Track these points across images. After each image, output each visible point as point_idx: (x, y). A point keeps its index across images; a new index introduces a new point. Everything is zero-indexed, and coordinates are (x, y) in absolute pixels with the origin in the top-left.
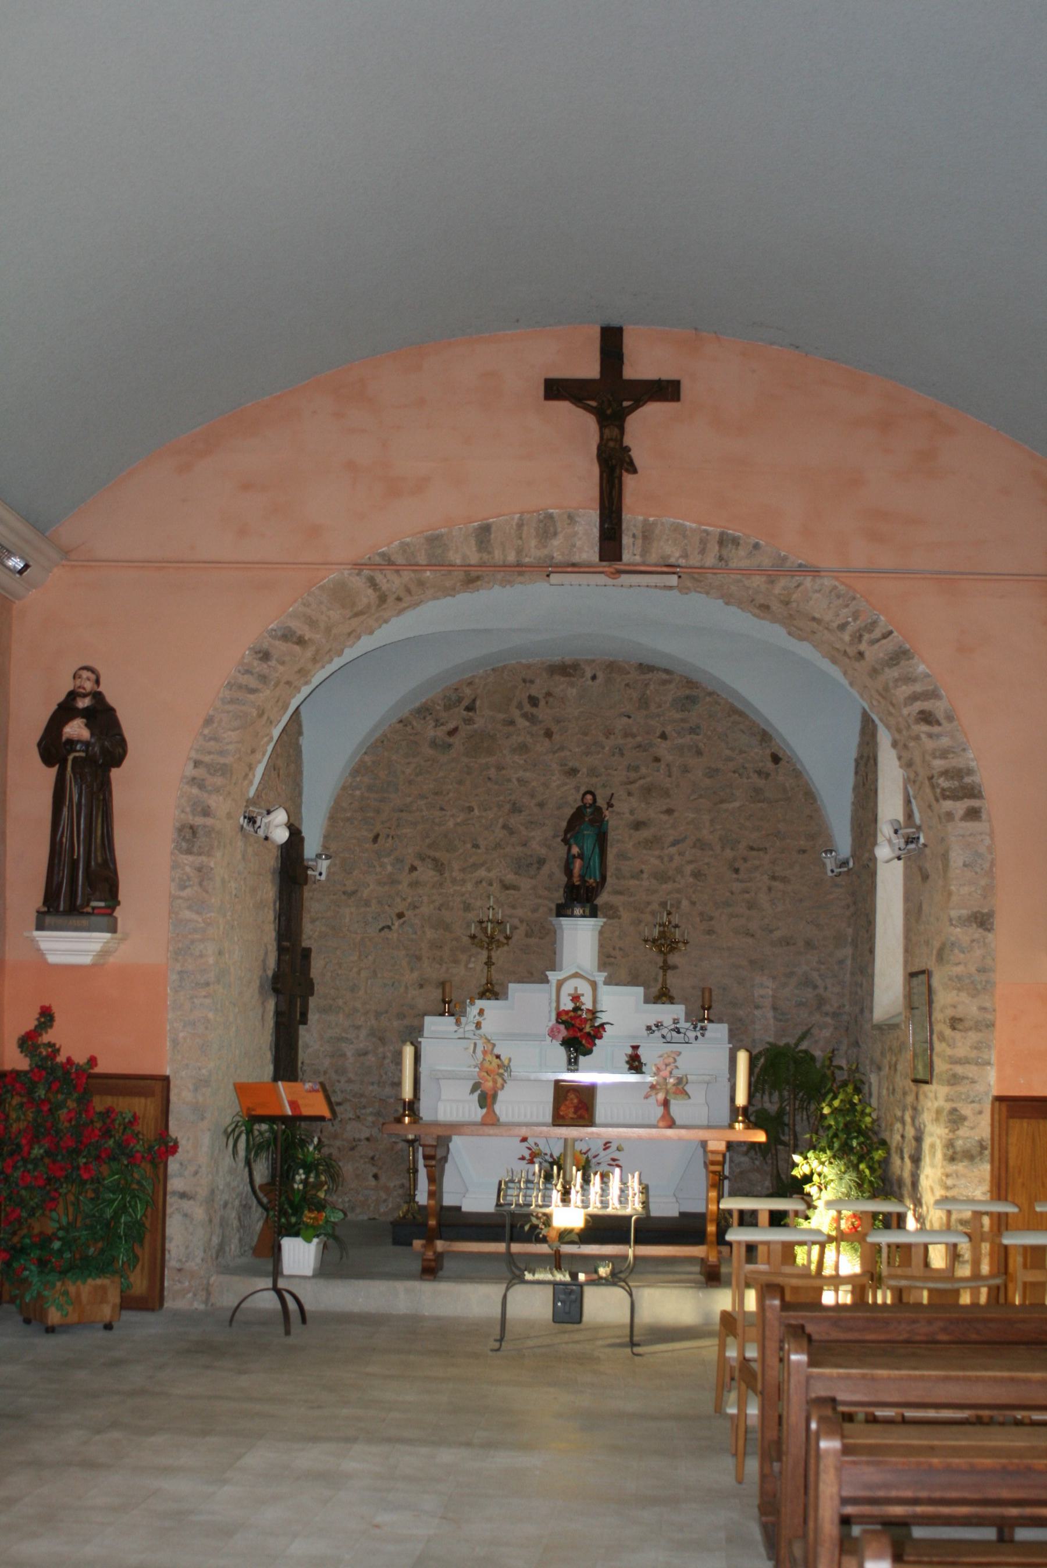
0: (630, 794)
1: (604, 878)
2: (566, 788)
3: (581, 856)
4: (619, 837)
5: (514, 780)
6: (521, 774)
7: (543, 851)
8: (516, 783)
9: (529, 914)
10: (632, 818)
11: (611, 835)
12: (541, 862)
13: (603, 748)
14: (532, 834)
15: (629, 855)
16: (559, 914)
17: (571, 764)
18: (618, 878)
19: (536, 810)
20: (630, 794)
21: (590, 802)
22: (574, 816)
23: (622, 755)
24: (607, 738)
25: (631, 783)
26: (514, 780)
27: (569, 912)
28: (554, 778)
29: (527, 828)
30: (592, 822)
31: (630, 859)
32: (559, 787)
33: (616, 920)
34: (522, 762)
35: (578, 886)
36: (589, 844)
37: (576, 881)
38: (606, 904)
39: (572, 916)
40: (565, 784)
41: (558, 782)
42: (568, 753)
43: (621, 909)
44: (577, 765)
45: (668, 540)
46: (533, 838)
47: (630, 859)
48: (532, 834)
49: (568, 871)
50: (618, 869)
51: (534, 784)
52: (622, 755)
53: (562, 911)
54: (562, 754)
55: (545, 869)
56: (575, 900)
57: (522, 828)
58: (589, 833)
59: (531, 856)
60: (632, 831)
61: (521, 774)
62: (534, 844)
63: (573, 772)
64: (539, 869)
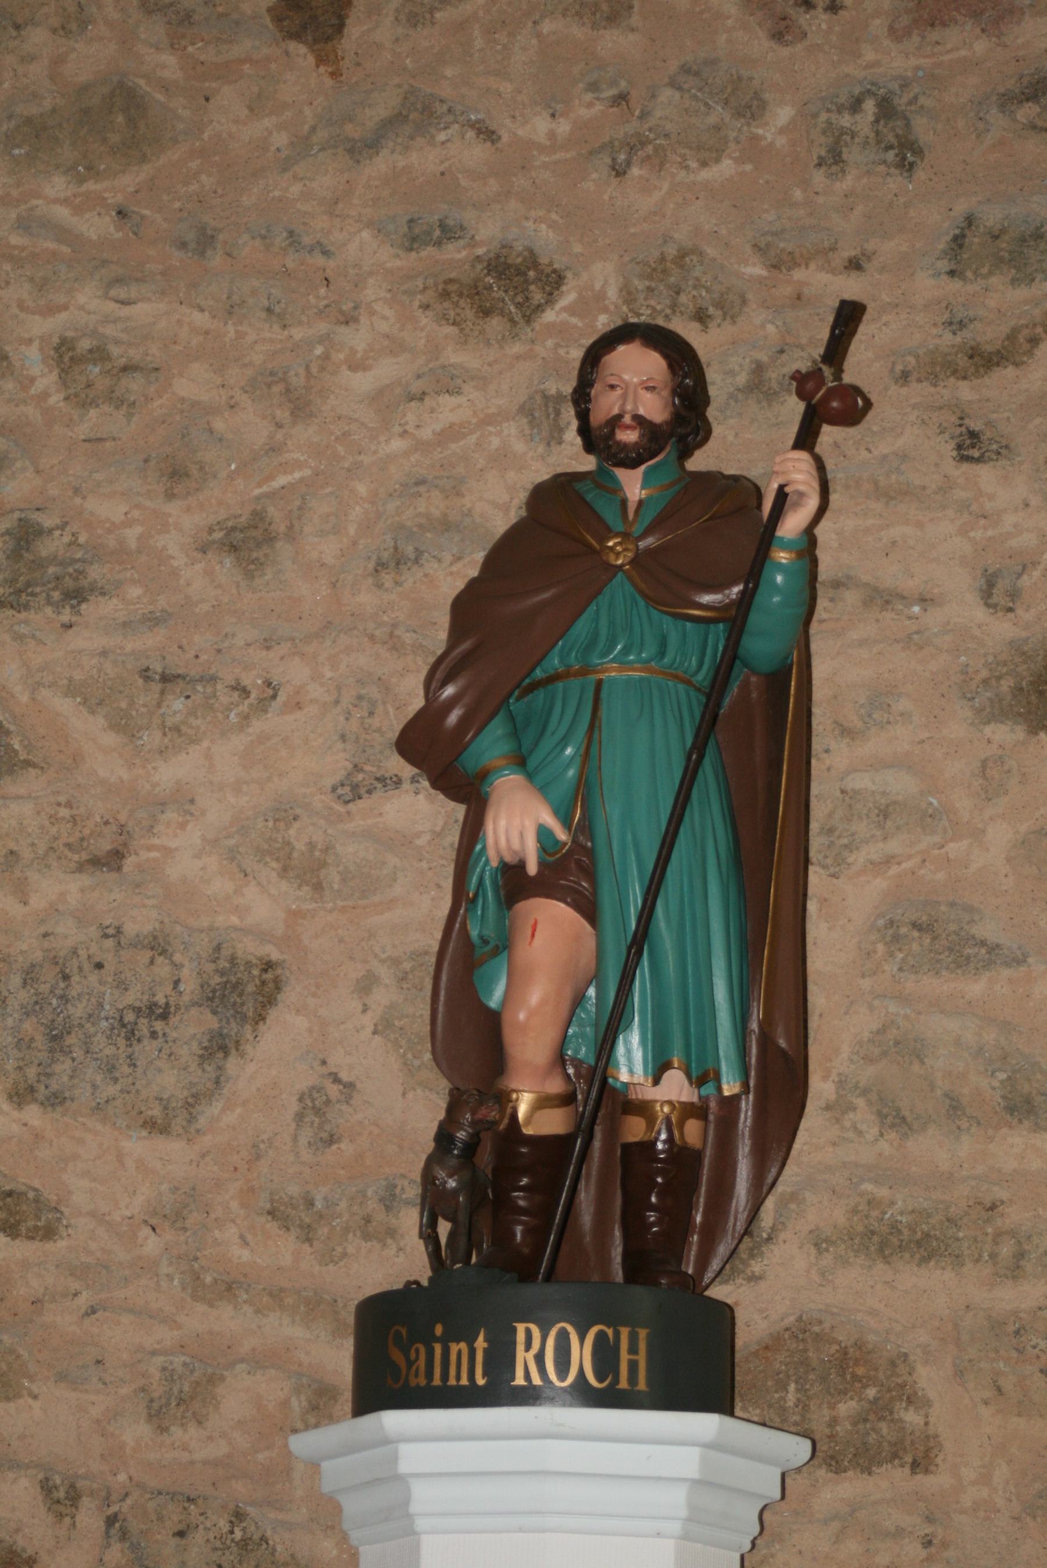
0: (971, 446)
1: (782, 1081)
2: (449, 410)
3: (568, 872)
4: (901, 784)
5: (32, 360)
6: (87, 306)
7: (257, 909)
8: (46, 380)
9: (135, 1432)
10: (1003, 630)
11: (840, 768)
12: (246, 991)
13: (752, 108)
14: (168, 773)
15: (988, 930)
16: (382, 1384)
17: (488, 231)
18: (896, 1120)
19: (207, 580)
20: (971, 446)
21: (655, 408)
22: (513, 560)
23: (907, 154)
24: (782, 32)
25: (984, 360)
26: (32, 360)
27: (467, 1359)
28: (357, 339)
29: (124, 725)
30: (665, 580)
31: (992, 955)
32: (388, 402)
33: (891, 1480)
34: (96, 226)
35: (555, 1151)
36: (644, 754)
37: (531, 1105)
38: (803, 1332)
39: (498, 1390)
40: (448, 383)
41: (387, 370)
42: (474, 153)
43: (928, 1378)
44: (543, 236)
45: (977, 371)
46: (184, 800)
47: (992, 955)
48: (168, 773)
49: (471, 1042)
50: (902, 1047)
51: (193, 384)
52: (907, 154)
53: (400, 1356)
54: (424, 159)
55: (276, 1055)
56: (525, 1269)
57: (88, 728)
58: (634, 662)
59: (158, 946)
60: (1005, 734)
61: (87, 306)
62: (183, 853)
63: (511, 285)
64: (219, 1047)
